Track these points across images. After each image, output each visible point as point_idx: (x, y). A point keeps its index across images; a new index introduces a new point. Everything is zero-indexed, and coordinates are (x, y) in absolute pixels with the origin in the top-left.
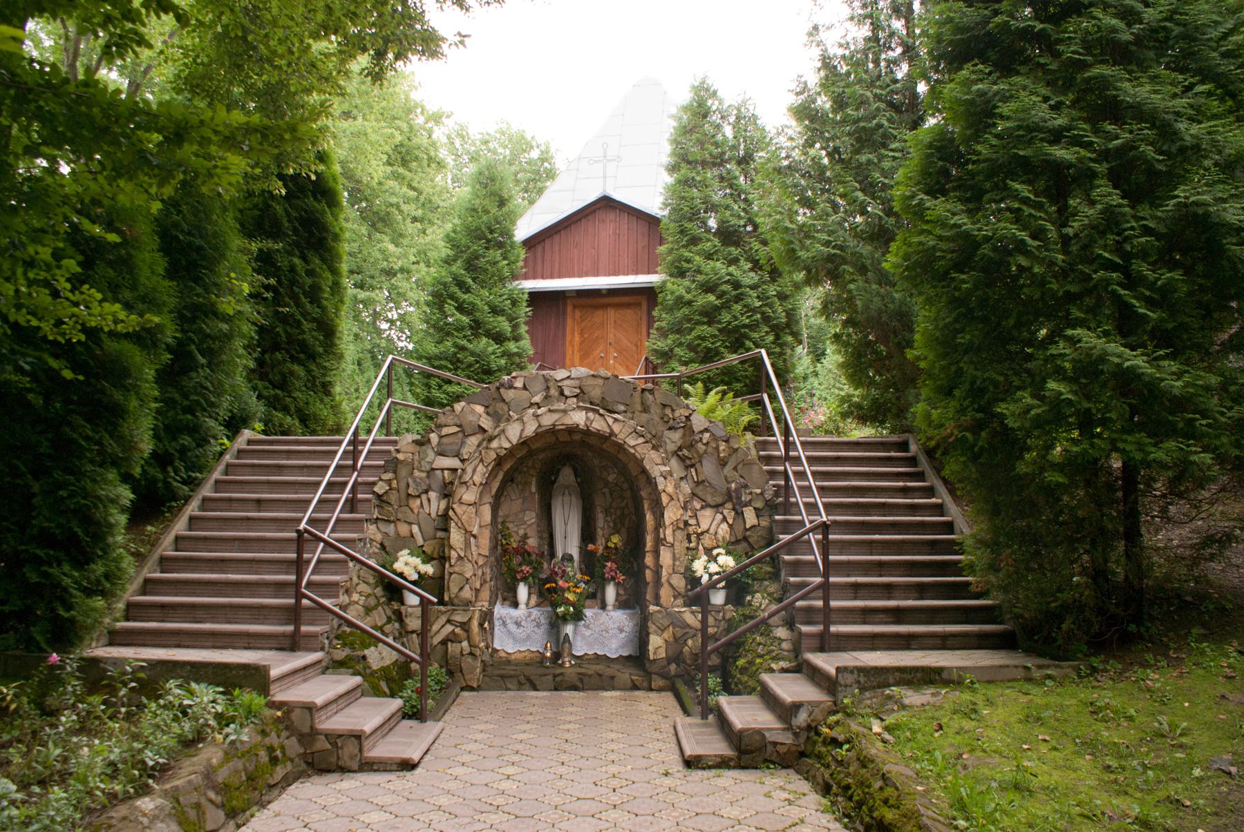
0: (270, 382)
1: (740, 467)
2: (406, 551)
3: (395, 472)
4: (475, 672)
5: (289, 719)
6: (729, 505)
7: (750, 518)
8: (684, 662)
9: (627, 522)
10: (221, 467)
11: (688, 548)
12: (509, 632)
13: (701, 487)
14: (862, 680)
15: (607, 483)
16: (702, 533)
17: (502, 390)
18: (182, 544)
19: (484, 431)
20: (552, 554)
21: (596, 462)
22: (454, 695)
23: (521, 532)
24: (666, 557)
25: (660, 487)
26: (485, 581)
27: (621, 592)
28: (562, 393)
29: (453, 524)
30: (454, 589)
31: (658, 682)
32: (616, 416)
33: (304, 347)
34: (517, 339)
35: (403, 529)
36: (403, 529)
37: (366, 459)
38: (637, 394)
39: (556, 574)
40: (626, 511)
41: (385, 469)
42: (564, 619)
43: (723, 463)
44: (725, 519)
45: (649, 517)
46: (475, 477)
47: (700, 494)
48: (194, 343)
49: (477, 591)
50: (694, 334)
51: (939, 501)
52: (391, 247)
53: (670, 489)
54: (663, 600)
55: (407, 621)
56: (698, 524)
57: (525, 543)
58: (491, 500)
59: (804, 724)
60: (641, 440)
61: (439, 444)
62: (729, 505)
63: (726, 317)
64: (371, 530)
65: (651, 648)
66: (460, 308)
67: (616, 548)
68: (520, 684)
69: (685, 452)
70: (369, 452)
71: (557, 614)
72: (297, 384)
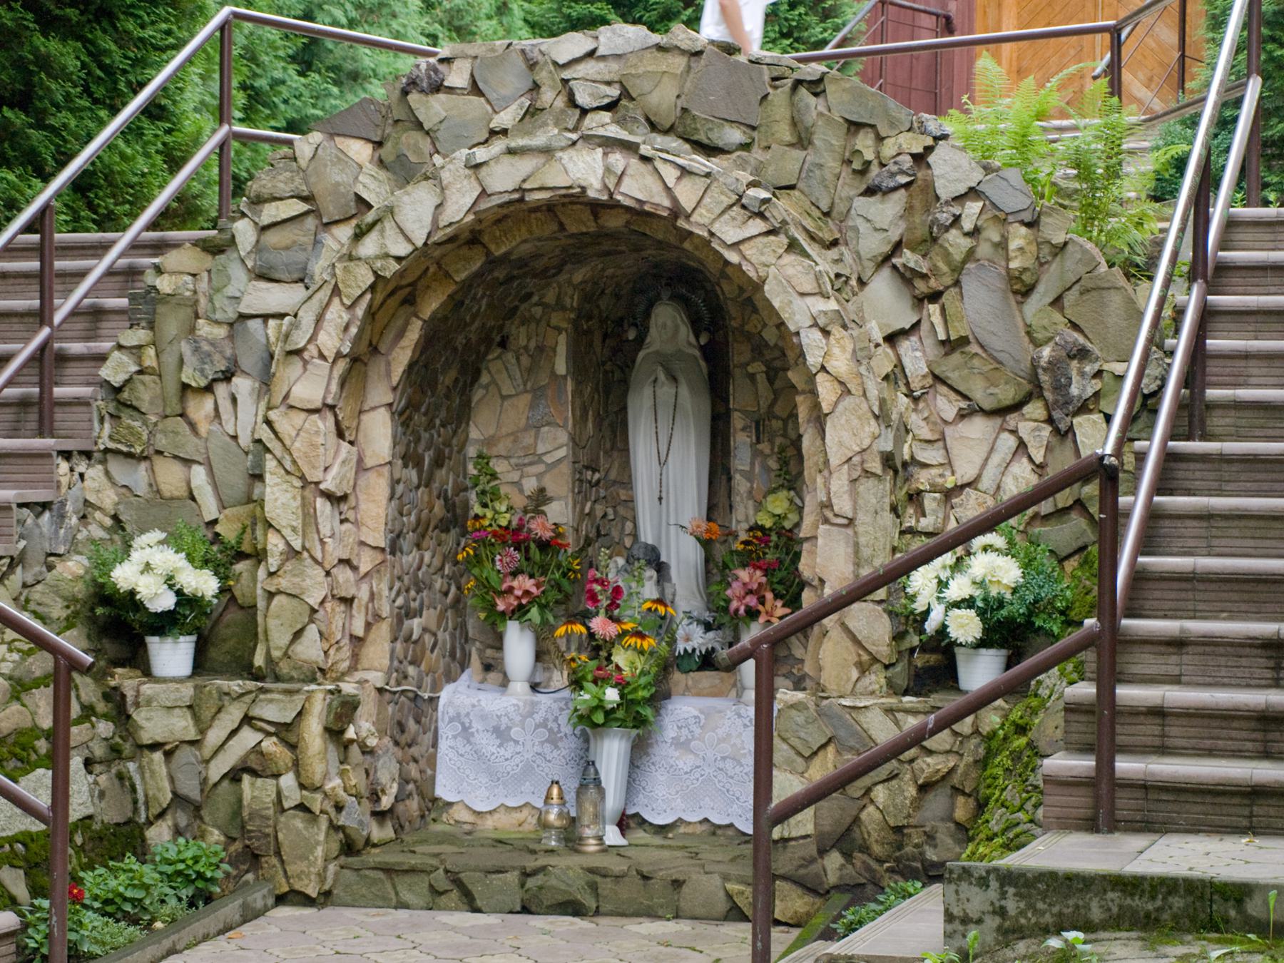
1: (1070, 298)
2: (157, 535)
3: (151, 326)
4: (311, 853)
6: (1035, 409)
8: (865, 849)
12: (479, 756)
13: (956, 357)
14: (1012, 905)
16: (960, 488)
23: (530, 485)
25: (813, 360)
30: (279, 637)
35: (170, 476)
36: (170, 476)
38: (779, 97)
41: (131, 318)
43: (1022, 289)
46: (322, 338)
47: (954, 377)
49: (357, 641)
53: (840, 363)
55: (139, 716)
56: (949, 464)
60: (757, 226)
61: (258, 248)
68: (435, 892)
69: (908, 258)
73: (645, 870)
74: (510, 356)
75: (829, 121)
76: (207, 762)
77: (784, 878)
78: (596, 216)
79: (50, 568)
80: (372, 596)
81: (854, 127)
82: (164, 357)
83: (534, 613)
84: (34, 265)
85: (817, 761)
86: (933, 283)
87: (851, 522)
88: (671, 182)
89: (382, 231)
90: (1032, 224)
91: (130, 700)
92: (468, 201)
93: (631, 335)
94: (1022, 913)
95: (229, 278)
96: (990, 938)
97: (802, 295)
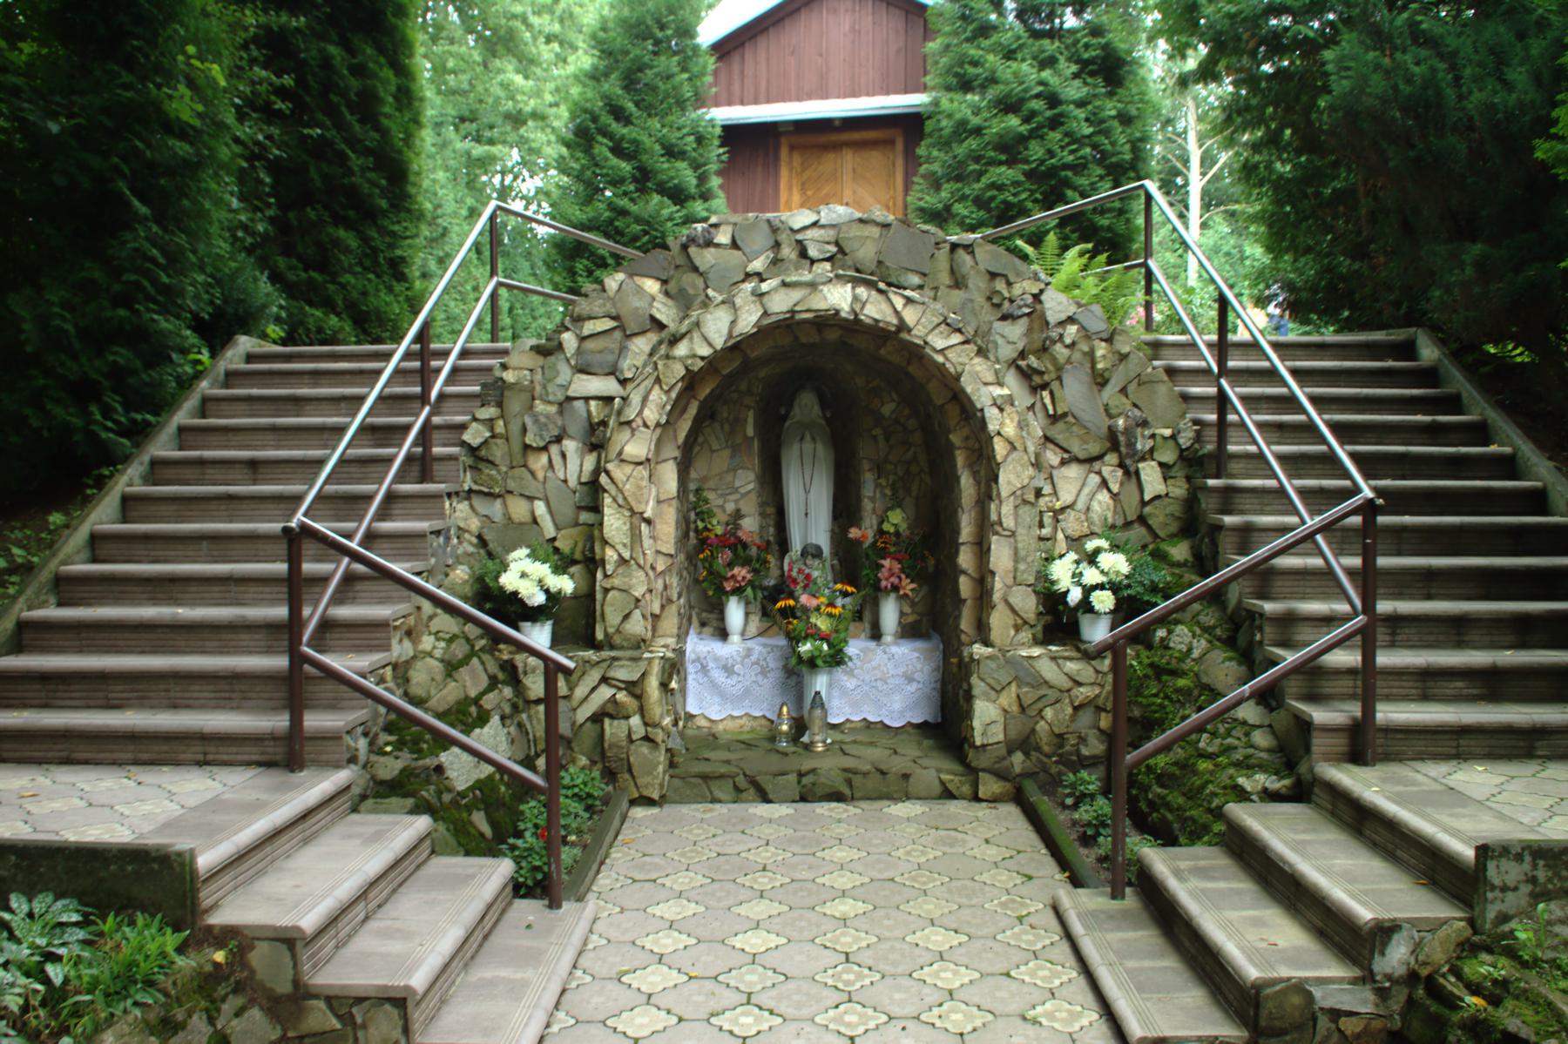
0: (300, 258)
1: (1132, 388)
2: (522, 552)
3: (500, 405)
4: (653, 771)
5: (245, 965)
7: (1151, 476)
8: (1038, 749)
9: (915, 487)
10: (191, 403)
11: (1041, 539)
13: (1060, 425)
14: (1541, 875)
15: (879, 419)
16: (1063, 509)
17: (692, 250)
18: (106, 549)
19: (660, 326)
20: (783, 545)
21: (860, 381)
22: (616, 822)
23: (730, 507)
24: (1001, 556)
25: (992, 427)
26: (670, 601)
27: (907, 610)
28: (803, 254)
29: (608, 500)
30: (613, 618)
31: (990, 786)
32: (908, 293)
33: (356, 199)
34: (706, 196)
35: (519, 509)
36: (519, 509)
37: (448, 382)
38: (943, 254)
39: (795, 581)
40: (914, 469)
41: (481, 399)
42: (812, 663)
43: (1101, 381)
44: (1104, 483)
45: (966, 482)
46: (647, 412)
47: (1059, 438)
48: (124, 176)
50: (984, 180)
51: (1507, 450)
52: (519, 79)
53: (1010, 430)
54: (995, 635)
56: (1055, 493)
57: (738, 527)
58: (677, 453)
59: (1401, 971)
60: (956, 338)
61: (579, 351)
62: (1112, 458)
63: (1036, 151)
64: (460, 513)
65: (976, 723)
66: (617, 151)
67: (897, 534)
68: (738, 790)
69: (1033, 361)
70: (455, 370)
71: (799, 657)
72: (346, 260)
73: (883, 767)
74: (717, 425)
75: (978, 271)
76: (575, 710)
77: (984, 770)
78: (820, 331)
79: (447, 575)
80: (665, 587)
81: (993, 275)
82: (510, 427)
83: (749, 591)
84: (417, 364)
85: (1004, 693)
86: (1046, 377)
87: (1013, 534)
88: (899, 307)
89: (691, 339)
90: (1109, 340)
91: (520, 670)
92: (754, 318)
93: (783, 411)
94: (1550, 880)
95: (558, 373)
96: (1524, 901)
97: (986, 384)
